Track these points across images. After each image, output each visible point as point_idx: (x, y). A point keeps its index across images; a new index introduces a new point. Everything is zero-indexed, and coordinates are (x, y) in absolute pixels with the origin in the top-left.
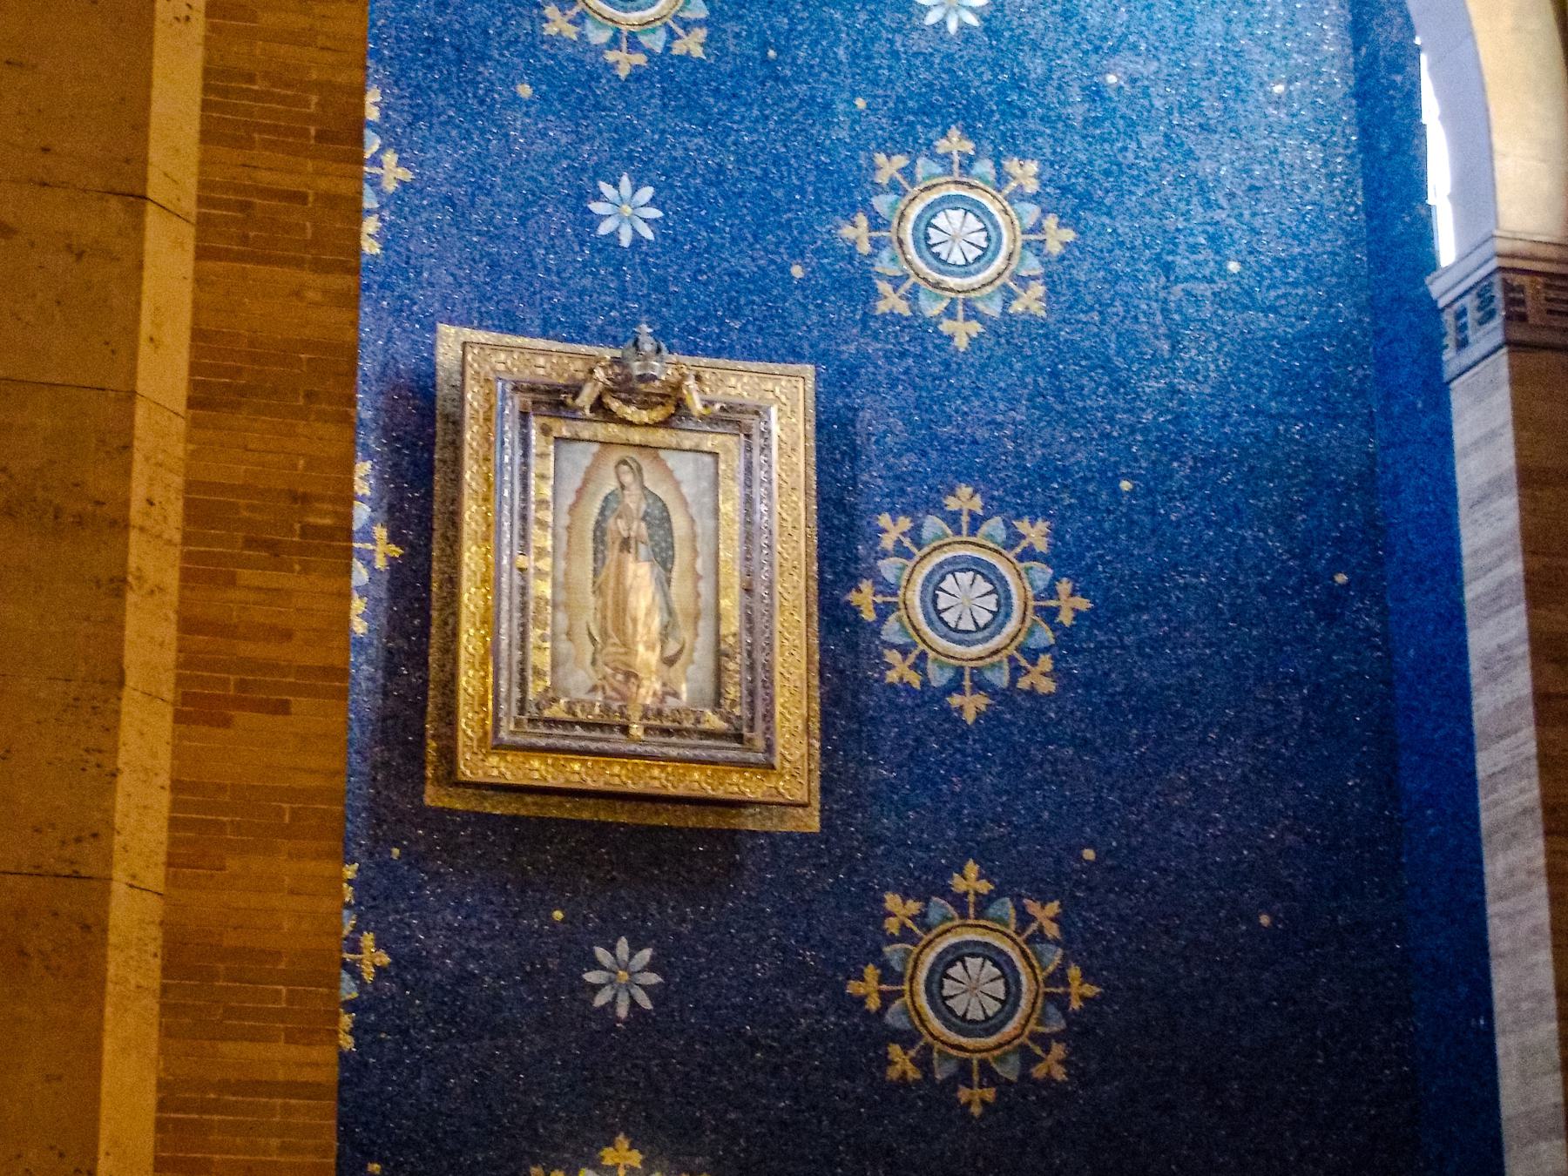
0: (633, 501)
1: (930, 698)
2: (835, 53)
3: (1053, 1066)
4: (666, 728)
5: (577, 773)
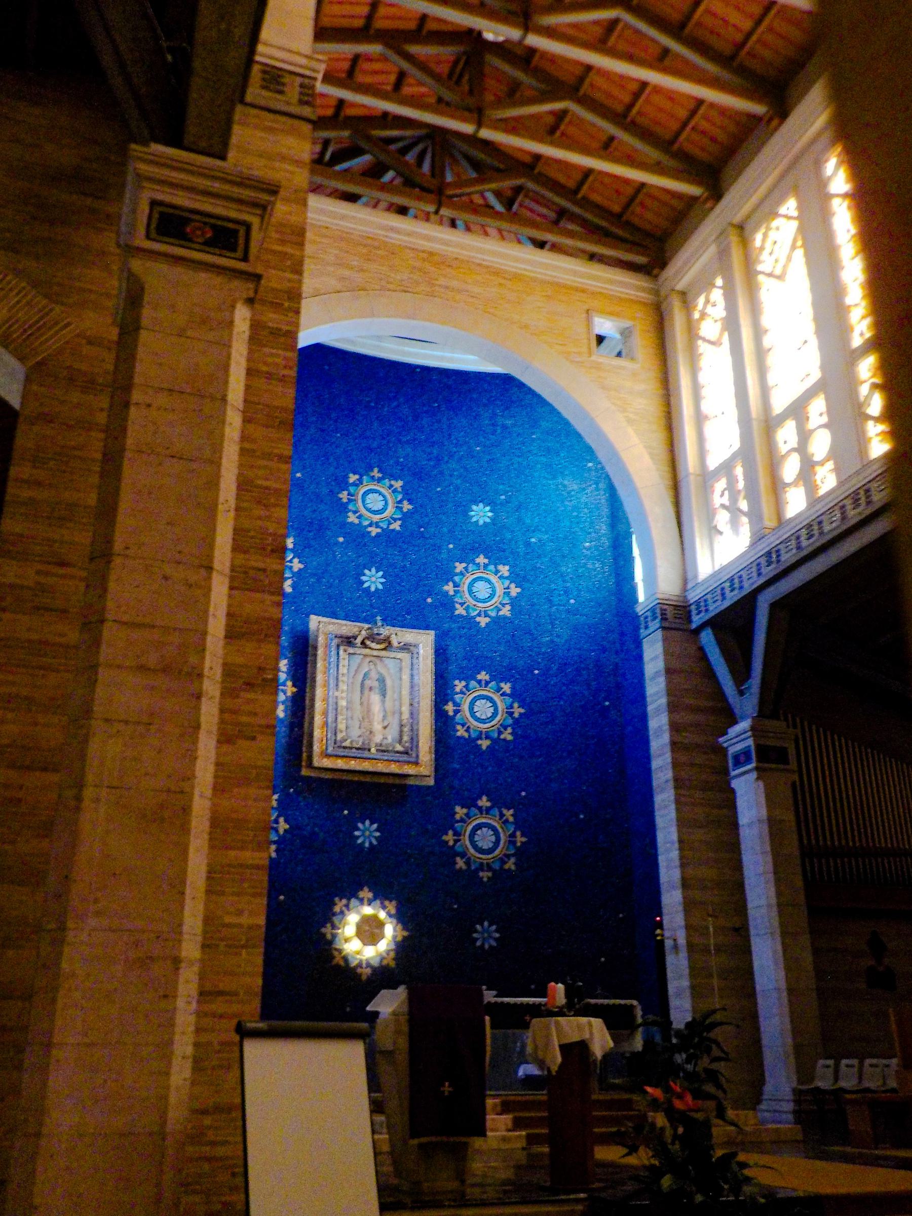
0: (374, 675)
5: (353, 765)
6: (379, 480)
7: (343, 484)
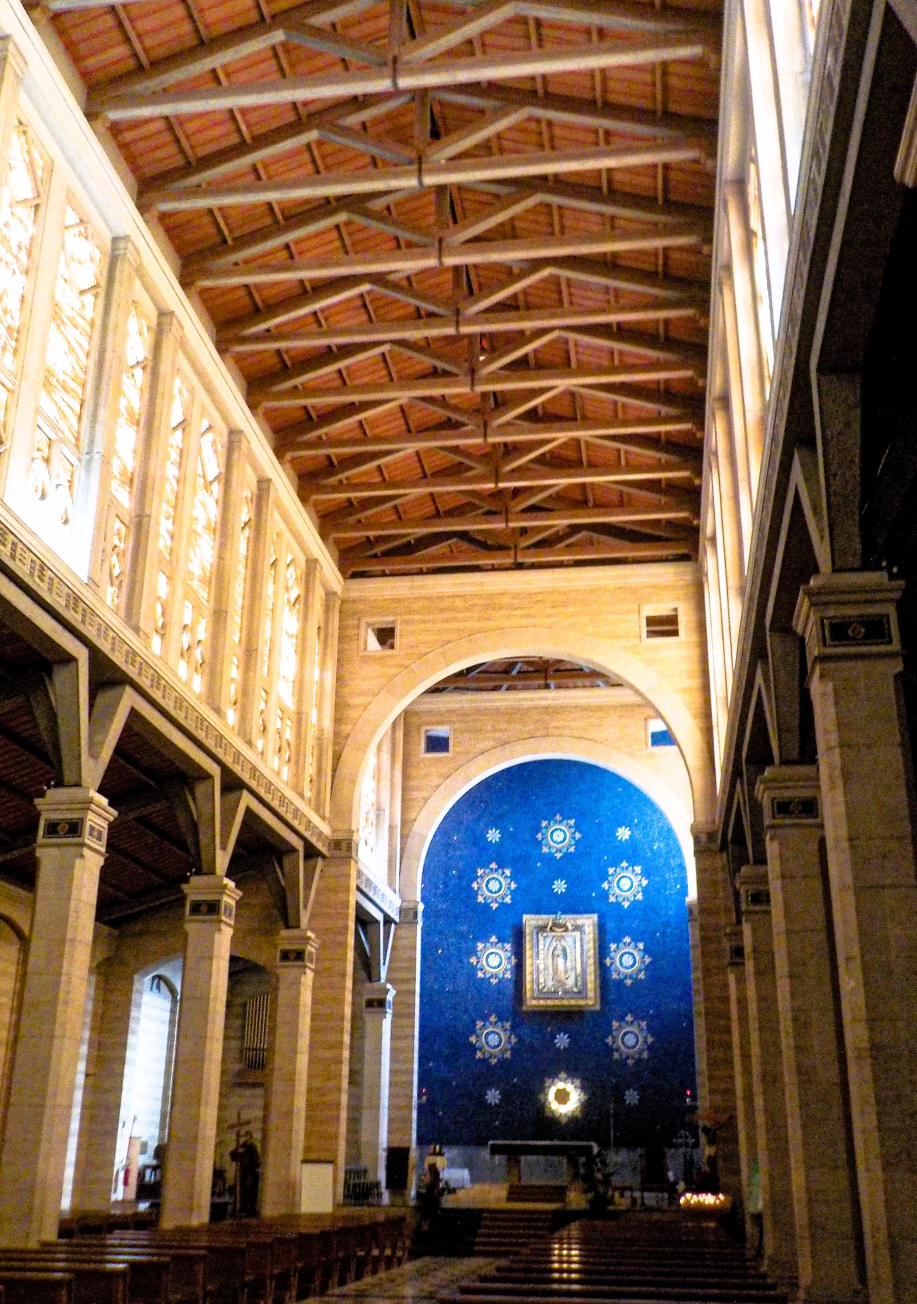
0: (559, 947)
1: (621, 981)
2: (616, 1165)
3: (645, 1055)
4: (566, 992)
5: (550, 1002)
6: (560, 822)
7: (538, 829)
